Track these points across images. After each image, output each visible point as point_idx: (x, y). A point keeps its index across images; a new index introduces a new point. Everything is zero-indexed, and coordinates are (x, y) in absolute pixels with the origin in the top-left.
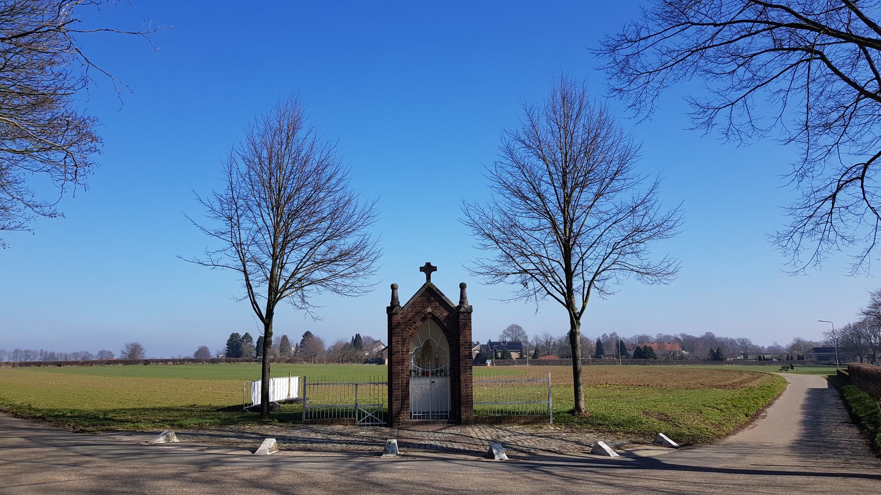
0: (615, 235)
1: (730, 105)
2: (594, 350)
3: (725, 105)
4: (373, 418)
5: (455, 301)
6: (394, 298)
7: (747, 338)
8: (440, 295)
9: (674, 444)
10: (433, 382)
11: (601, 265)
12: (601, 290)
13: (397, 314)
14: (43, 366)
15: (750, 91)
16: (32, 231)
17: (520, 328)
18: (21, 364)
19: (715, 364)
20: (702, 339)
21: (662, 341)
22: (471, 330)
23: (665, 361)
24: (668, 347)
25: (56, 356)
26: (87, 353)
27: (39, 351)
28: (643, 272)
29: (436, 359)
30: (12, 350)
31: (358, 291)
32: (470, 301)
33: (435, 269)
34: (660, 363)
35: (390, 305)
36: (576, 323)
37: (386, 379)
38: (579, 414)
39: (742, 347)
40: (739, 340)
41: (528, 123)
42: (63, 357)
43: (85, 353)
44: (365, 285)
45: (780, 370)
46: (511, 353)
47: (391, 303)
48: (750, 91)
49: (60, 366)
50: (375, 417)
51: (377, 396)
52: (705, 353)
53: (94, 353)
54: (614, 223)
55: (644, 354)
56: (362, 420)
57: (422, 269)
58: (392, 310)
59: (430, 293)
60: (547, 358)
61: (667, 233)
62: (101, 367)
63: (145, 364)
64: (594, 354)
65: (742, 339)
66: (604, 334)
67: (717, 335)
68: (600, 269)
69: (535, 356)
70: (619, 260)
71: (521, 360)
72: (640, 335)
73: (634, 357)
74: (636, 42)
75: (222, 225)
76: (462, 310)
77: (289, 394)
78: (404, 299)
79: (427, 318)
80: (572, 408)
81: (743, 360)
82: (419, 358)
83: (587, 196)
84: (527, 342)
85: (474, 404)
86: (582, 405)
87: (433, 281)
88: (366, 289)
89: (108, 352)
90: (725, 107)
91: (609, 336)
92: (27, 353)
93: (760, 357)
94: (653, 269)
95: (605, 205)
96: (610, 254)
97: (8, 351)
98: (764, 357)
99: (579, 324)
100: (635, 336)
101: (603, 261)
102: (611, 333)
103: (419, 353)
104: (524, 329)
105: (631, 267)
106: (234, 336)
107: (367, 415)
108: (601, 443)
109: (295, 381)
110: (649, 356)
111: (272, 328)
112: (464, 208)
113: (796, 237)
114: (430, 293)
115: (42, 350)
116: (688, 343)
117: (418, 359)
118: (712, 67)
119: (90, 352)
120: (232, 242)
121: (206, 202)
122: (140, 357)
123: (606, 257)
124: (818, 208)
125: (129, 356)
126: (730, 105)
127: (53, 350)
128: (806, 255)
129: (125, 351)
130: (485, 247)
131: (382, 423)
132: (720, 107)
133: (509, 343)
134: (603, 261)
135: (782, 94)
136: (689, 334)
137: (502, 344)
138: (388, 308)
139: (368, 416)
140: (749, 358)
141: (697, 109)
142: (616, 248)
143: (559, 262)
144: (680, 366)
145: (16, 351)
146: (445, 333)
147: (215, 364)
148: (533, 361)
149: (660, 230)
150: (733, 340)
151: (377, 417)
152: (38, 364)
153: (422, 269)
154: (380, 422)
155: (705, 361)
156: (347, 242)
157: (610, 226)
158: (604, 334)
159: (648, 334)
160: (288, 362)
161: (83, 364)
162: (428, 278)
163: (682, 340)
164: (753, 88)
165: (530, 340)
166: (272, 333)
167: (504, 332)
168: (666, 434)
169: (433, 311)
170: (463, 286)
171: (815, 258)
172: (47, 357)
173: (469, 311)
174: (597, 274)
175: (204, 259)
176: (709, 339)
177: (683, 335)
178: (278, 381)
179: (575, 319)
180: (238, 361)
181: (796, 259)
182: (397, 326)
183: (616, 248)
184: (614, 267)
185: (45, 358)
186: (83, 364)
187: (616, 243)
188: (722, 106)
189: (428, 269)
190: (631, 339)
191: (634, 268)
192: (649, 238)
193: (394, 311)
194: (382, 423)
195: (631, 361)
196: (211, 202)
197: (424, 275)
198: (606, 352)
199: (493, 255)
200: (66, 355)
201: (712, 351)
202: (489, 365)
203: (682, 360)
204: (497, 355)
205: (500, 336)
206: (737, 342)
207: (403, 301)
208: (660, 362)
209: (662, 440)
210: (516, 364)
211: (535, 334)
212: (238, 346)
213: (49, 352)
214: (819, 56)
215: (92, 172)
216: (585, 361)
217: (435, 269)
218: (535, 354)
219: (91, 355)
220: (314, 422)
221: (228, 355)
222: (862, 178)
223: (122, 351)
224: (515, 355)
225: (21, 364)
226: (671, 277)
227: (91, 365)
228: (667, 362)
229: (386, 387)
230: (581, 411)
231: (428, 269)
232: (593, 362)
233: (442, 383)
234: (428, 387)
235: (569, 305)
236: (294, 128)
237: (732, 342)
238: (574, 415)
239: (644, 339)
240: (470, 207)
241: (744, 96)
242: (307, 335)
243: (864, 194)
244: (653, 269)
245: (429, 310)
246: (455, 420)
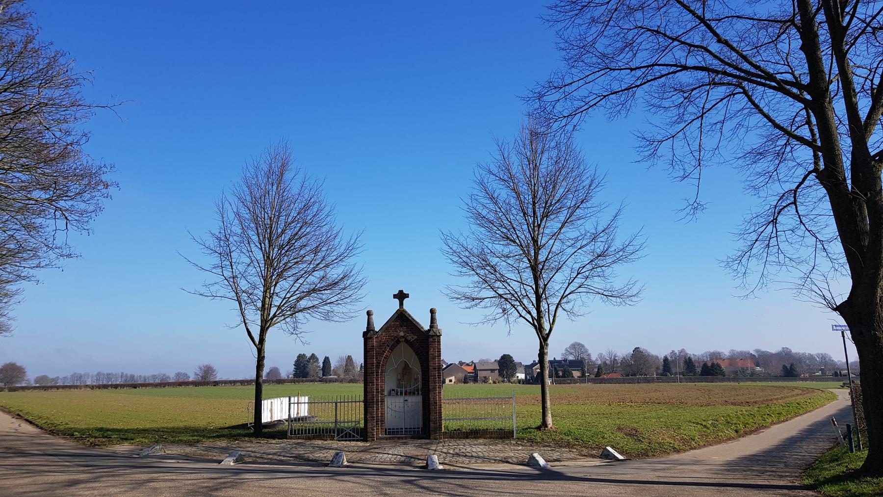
0: (584, 258)
1: (671, 137)
2: (661, 368)
3: (667, 138)
4: (357, 434)
5: (426, 326)
6: (369, 323)
7: (826, 352)
8: (412, 321)
9: (620, 457)
10: (406, 400)
11: (567, 288)
12: (570, 312)
13: (372, 338)
14: (119, 388)
15: (688, 125)
16: (61, 269)
17: (583, 346)
18: (99, 387)
19: (789, 380)
20: (778, 355)
21: (734, 358)
22: (440, 351)
23: (734, 378)
24: (740, 364)
25: (135, 378)
26: (164, 375)
27: (120, 374)
28: (608, 295)
29: (415, 379)
30: (95, 373)
31: (345, 317)
32: (440, 324)
33: (407, 296)
34: (729, 380)
36: (543, 343)
37: (362, 399)
38: (545, 430)
39: (821, 363)
40: (818, 355)
41: (500, 158)
42: (142, 379)
43: (162, 375)
44: (352, 311)
45: (841, 386)
46: (573, 372)
47: (367, 328)
48: (688, 125)
49: (136, 388)
50: (352, 433)
51: (354, 415)
52: (777, 369)
53: (172, 376)
54: (580, 249)
55: (712, 372)
56: (344, 433)
57: (395, 296)
58: (367, 335)
59: (402, 318)
60: (610, 376)
61: (632, 257)
62: (173, 389)
63: (214, 386)
64: (660, 371)
65: (822, 354)
66: (673, 351)
67: (794, 350)
68: (567, 293)
69: (598, 374)
70: (585, 283)
71: (583, 379)
72: (712, 351)
73: (702, 374)
74: (561, 88)
75: (215, 260)
76: (431, 333)
77: (298, 413)
78: (378, 324)
79: (400, 342)
80: (540, 423)
81: (821, 376)
82: (399, 378)
83: (552, 225)
84: (590, 359)
85: (442, 421)
86: (549, 420)
87: (405, 307)
88: (353, 315)
89: (184, 373)
90: (667, 140)
91: (678, 353)
92: (108, 376)
93: (836, 373)
94: (619, 291)
95: (570, 233)
96: (575, 278)
97: (91, 374)
98: (840, 372)
99: (547, 345)
100: (706, 353)
101: (568, 286)
102: (680, 349)
103: (400, 374)
104: (587, 346)
105: (597, 290)
106: (301, 357)
107: (345, 431)
108: (536, 455)
109: (307, 398)
110: (717, 373)
111: (264, 352)
112: (443, 238)
113: (744, 260)
114: (402, 318)
115: (122, 373)
116: (762, 359)
117: (398, 379)
118: (655, 103)
119: (167, 375)
120: (223, 275)
121: (200, 241)
122: (212, 379)
123: (571, 281)
124: (762, 232)
125: (202, 377)
126: (671, 137)
127: (133, 373)
128: (753, 279)
129: (198, 373)
130: (465, 274)
131: (359, 438)
132: (663, 140)
133: (571, 362)
134: (568, 286)
135: (719, 125)
136: (763, 349)
137: (563, 362)
138: (364, 332)
140: (827, 374)
141: (644, 143)
142: (581, 272)
143: (531, 286)
144: (749, 383)
145: (99, 374)
146: (417, 355)
147: (280, 385)
148: (596, 380)
149: (624, 255)
150: (812, 356)
151: (354, 433)
152: (116, 386)
153: (395, 296)
154: (357, 437)
155: (776, 378)
156: (335, 273)
157: (575, 252)
158: (673, 351)
159: (720, 350)
160: (351, 381)
161: (156, 385)
162: (401, 304)
163: (757, 356)
164: (690, 121)
165: (594, 358)
166: (264, 357)
167: (566, 350)
168: (613, 447)
170: (432, 312)
171: (761, 281)
172: (128, 379)
173: (438, 334)
174: (562, 298)
175: (203, 290)
176: (785, 355)
177: (757, 351)
178: (266, 401)
179: (544, 339)
180: (302, 381)
181: (745, 282)
182: (372, 349)
183: (581, 272)
184: (580, 290)
185: (126, 381)
186: (156, 385)
187: (580, 268)
188: (664, 139)
189: (401, 296)
190: (702, 356)
191: (600, 291)
192: (614, 262)
193: (369, 335)
194: (359, 438)
195: (699, 379)
196: (204, 241)
197: (397, 301)
198: (673, 370)
199: (468, 282)
200: (145, 377)
201: (785, 367)
202: (550, 384)
203: (753, 377)
204: (559, 374)
205: (563, 354)
206: (816, 357)
207: (378, 326)
208: (729, 378)
209: (607, 453)
210: (577, 383)
211: (600, 352)
212: (305, 367)
213: (129, 375)
214: (742, 91)
215: (93, 219)
216: (649, 379)
217: (407, 296)
218: (598, 372)
219: (169, 377)
220: (297, 438)
221: (295, 375)
222: (795, 203)
223: (195, 373)
224: (576, 374)
225: (99, 387)
226: (634, 299)
227: (164, 387)
228: (736, 379)
229: (362, 404)
230: (547, 427)
231: (401, 296)
232: (658, 380)
233: (415, 401)
234: (402, 405)
235: (539, 329)
236: (284, 167)
237: (811, 357)
238: (540, 430)
239: (715, 355)
240: (448, 238)
241: (683, 129)
242: (313, 354)
243: (800, 218)
244: (619, 291)
245: (402, 334)
246: (425, 435)
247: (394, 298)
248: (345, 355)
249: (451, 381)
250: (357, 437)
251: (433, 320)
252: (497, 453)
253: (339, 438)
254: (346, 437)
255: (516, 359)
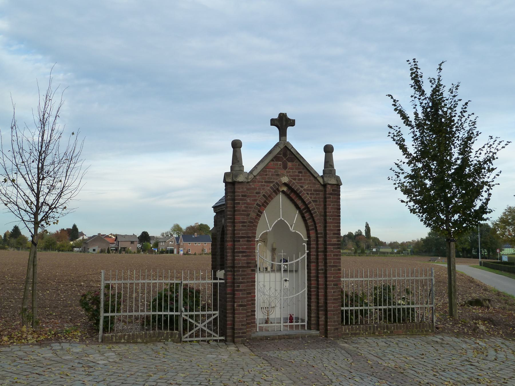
6: (237, 159)
33: (292, 123)
35: (229, 170)
57: (273, 122)
139: (197, 328)
153: (273, 122)
154: (214, 336)
162: (283, 134)
169: (290, 181)
189: (387, 95)
217: (292, 123)
247: (271, 125)
248: (73, 224)
249: (94, 250)
250: (214, 336)
251: (329, 163)
252: (483, 365)
253: (187, 338)
254: (197, 336)
255: (150, 234)
